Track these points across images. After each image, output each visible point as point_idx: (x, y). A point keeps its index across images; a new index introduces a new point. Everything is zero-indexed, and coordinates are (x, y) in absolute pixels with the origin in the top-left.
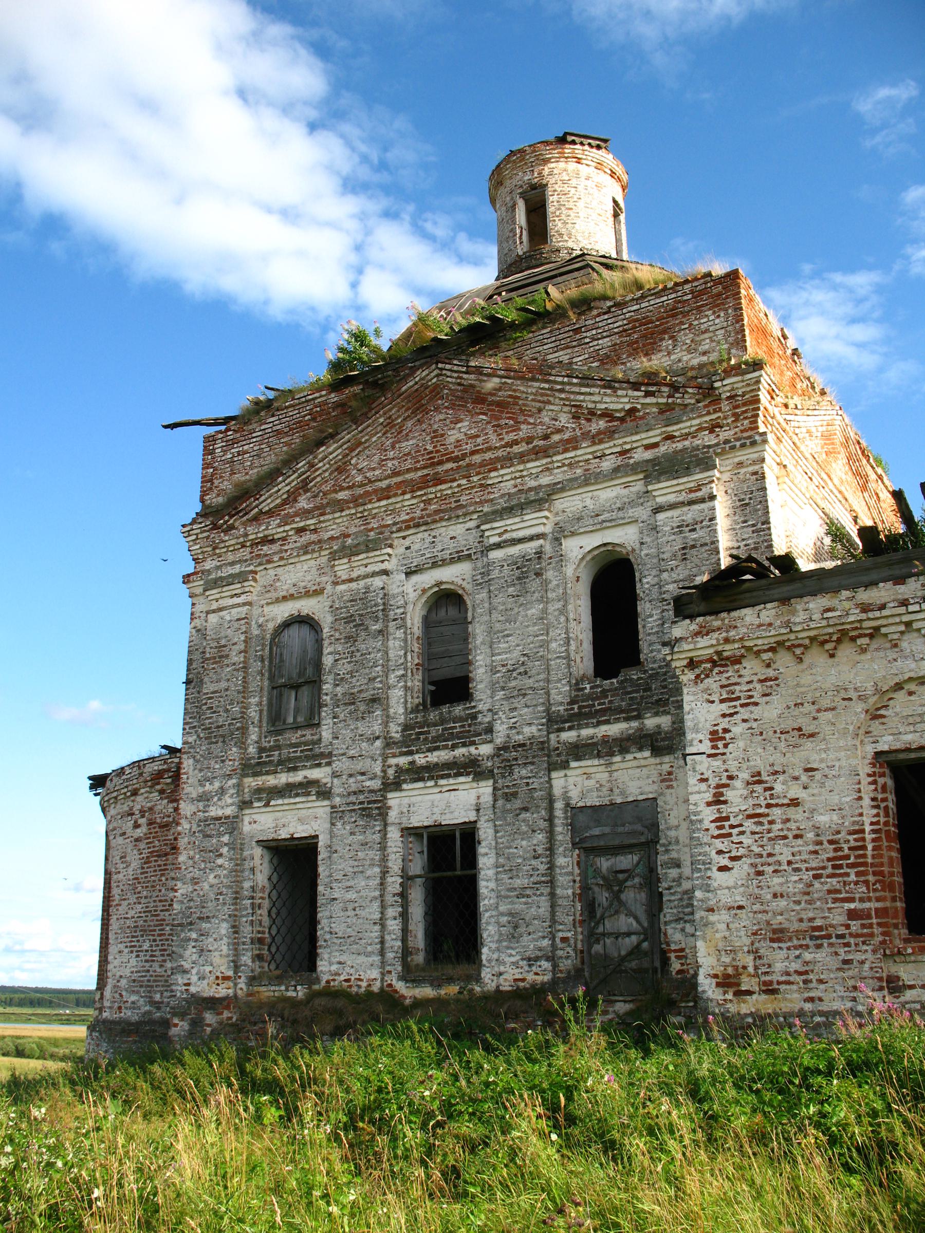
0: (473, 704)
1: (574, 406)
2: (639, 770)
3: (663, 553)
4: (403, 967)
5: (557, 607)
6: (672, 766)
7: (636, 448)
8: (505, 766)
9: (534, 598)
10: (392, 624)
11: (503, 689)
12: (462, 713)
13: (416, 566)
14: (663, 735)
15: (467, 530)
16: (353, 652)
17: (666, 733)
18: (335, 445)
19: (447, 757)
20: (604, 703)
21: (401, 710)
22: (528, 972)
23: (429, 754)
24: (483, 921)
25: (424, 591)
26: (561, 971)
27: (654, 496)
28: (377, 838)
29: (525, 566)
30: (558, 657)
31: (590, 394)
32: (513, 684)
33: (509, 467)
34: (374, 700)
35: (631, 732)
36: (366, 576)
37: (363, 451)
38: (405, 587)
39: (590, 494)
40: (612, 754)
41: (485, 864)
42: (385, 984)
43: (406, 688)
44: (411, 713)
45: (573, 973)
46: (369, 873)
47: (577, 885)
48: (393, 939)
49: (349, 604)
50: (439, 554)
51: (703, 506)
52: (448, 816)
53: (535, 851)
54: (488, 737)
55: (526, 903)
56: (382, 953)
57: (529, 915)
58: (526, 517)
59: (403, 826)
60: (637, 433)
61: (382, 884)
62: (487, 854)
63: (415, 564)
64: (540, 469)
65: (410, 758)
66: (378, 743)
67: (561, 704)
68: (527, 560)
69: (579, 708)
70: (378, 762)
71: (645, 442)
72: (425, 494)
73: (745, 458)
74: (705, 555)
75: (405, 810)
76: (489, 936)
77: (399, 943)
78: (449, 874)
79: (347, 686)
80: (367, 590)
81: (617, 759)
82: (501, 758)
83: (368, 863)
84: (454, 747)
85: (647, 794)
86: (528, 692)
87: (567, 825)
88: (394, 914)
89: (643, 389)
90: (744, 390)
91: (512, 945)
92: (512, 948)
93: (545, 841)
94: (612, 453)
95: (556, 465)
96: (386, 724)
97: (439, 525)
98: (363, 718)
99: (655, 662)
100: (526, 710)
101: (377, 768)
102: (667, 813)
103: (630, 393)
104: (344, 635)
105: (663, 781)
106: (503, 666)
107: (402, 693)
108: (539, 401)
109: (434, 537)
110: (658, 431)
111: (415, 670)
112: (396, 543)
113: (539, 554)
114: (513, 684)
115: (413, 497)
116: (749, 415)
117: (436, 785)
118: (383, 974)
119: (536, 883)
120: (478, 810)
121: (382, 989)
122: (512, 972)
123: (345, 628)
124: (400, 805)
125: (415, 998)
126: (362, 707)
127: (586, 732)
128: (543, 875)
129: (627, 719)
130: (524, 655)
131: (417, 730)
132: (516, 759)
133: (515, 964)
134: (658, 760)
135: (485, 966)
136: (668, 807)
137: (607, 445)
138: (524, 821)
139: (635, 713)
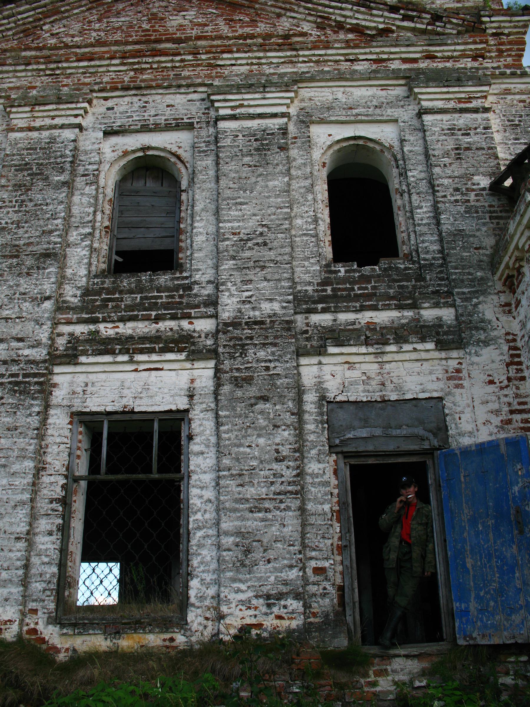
0: (185, 274)
1: (321, 17)
2: (419, 364)
3: (434, 150)
4: (57, 605)
5: (303, 184)
6: (460, 363)
7: (393, 59)
8: (235, 346)
9: (277, 171)
10: (78, 179)
11: (233, 258)
12: (169, 284)
13: (120, 126)
14: (446, 329)
15: (189, 101)
16: (23, 201)
17: (449, 327)
18: (28, 7)
19: (146, 330)
20: (366, 288)
21: (83, 272)
22: (266, 614)
23: (121, 325)
24: (193, 542)
25: (126, 153)
26: (315, 615)
27: (420, 99)
28: (34, 421)
29: (266, 139)
30: (304, 235)
31: (341, 9)
32: (248, 254)
33: (246, 52)
34: (47, 255)
35: (404, 321)
36: (55, 127)
37: (60, 20)
38: (101, 146)
39: (342, 89)
40: (386, 343)
41: (199, 466)
42: (25, 628)
43: (92, 250)
44: (96, 276)
45: (332, 616)
46: (16, 467)
47: (335, 500)
48: (43, 563)
49: (25, 152)
50: (151, 119)
51: (475, 116)
52: (145, 401)
53: (277, 451)
54: (211, 310)
55: (263, 520)
56: (25, 582)
57: (269, 535)
58: (268, 95)
59: (74, 409)
60: (396, 46)
61: (34, 484)
62: (202, 453)
63: (119, 124)
64: (282, 60)
65: (92, 327)
66: (48, 305)
67: (309, 283)
68: (268, 134)
69: (333, 290)
70: (44, 327)
71: (403, 56)
72: (138, 63)
73: (512, 86)
74: (482, 158)
75: (79, 390)
76: (202, 563)
77: (55, 569)
78: (141, 476)
79: (9, 237)
80: (53, 140)
81: (392, 348)
82: (229, 335)
83: (16, 454)
84: (157, 319)
85: (431, 391)
86: (267, 265)
87: (322, 422)
88: (49, 527)
89: (402, 12)
90: (510, 30)
91: (240, 576)
92: (240, 581)
93: (292, 439)
94: (366, 60)
95: (301, 59)
96: (60, 283)
97: (153, 92)
98: (28, 274)
99: (427, 252)
100: (265, 283)
101: (44, 335)
102: (457, 416)
103: (386, 14)
104: (13, 182)
105: (449, 379)
106: (234, 234)
107: (86, 252)
108: (281, 8)
109: (146, 102)
110: (420, 49)
111: (103, 233)
112: (95, 102)
113: (284, 131)
114: (248, 254)
115: (123, 64)
116: (513, 53)
117: (131, 361)
118: (23, 614)
119: (279, 494)
120: (191, 397)
121: (19, 636)
122: (240, 614)
123: (16, 176)
124: (71, 383)
125: (74, 650)
126: (29, 262)
127: (343, 317)
128: (289, 483)
129: (399, 307)
130: (263, 226)
131: (104, 296)
132: (251, 338)
133: (247, 604)
134: (443, 355)
135: (193, 605)
136: (459, 409)
137: (362, 51)
138: (262, 412)
139: (409, 302)
